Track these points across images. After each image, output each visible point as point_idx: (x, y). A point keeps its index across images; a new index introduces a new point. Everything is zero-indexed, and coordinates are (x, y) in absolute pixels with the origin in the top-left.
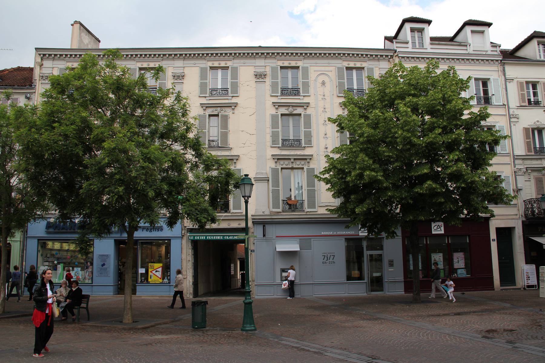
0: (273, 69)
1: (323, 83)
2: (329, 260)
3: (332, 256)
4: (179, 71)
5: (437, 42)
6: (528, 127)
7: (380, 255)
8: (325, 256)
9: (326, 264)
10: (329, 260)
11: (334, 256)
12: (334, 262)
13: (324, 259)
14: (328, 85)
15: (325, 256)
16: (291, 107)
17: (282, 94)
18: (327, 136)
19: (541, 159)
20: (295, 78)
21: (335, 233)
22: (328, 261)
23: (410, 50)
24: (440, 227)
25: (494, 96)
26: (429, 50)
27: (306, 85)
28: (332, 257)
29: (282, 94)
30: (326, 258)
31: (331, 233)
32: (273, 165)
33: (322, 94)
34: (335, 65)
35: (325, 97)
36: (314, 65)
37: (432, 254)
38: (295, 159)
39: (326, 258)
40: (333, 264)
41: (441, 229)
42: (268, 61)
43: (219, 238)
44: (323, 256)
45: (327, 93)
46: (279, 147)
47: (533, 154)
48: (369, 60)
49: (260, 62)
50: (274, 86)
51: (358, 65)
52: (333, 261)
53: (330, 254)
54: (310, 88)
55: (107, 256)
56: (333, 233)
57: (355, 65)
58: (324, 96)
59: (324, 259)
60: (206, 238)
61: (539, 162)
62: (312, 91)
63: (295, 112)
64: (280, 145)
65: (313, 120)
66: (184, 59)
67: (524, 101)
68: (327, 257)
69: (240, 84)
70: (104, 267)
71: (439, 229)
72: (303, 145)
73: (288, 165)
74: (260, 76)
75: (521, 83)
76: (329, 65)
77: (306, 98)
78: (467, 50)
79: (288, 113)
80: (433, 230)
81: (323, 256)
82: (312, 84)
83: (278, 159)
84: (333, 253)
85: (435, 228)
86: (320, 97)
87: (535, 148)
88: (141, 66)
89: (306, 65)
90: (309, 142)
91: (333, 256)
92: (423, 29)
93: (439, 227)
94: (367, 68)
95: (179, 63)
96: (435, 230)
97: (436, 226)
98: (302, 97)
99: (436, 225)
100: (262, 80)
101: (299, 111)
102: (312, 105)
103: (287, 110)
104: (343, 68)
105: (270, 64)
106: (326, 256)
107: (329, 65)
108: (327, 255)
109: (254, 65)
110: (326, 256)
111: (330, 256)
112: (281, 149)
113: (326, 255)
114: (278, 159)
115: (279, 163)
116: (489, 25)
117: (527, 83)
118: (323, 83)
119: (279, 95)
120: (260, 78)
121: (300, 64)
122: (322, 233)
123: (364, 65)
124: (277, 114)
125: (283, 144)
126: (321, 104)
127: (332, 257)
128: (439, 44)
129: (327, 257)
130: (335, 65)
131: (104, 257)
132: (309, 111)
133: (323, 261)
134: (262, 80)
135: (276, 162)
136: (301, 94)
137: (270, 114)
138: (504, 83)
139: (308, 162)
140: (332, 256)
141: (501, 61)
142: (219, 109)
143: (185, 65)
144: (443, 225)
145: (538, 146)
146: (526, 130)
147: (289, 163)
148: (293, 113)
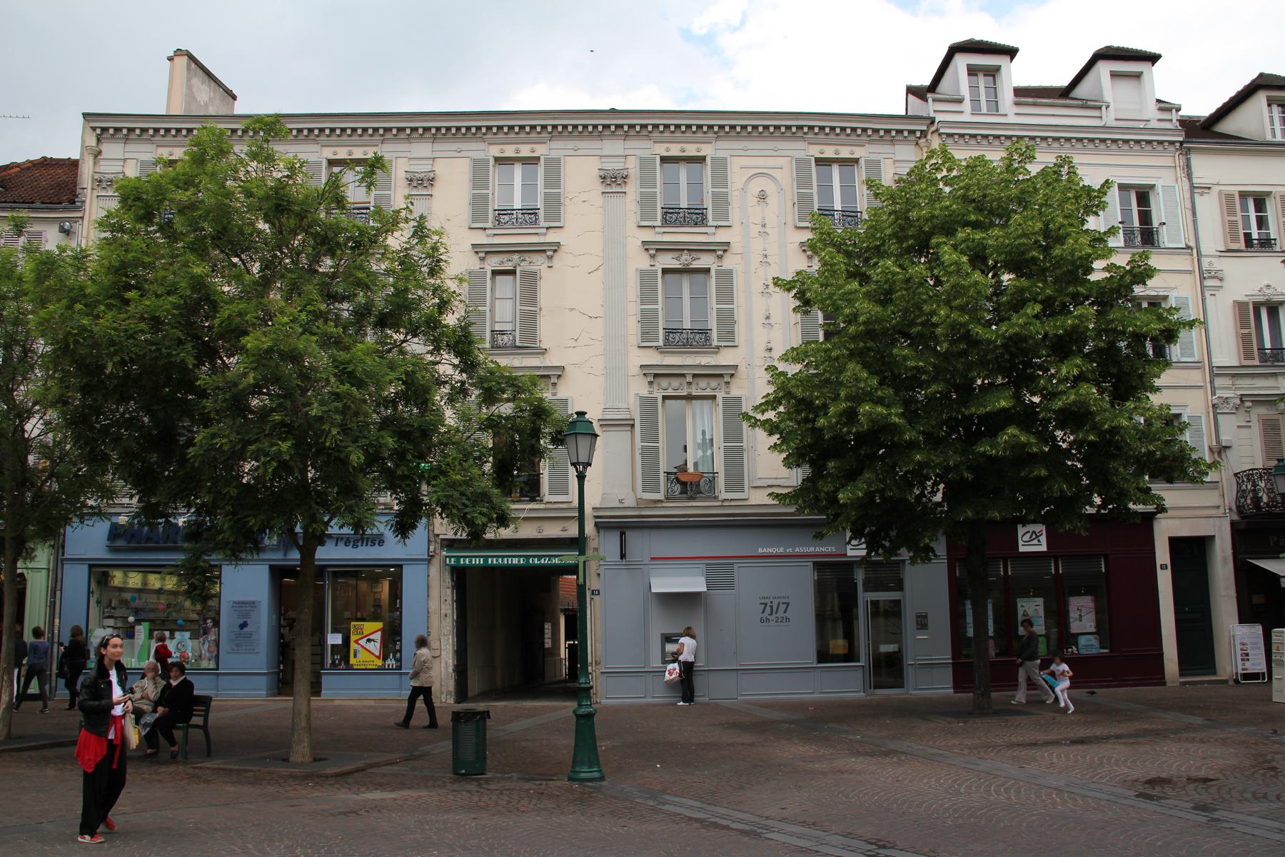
0: (645, 164)
1: (762, 197)
2: (776, 613)
3: (783, 603)
4: (421, 168)
5: (1030, 100)
6: (1246, 299)
7: (897, 603)
8: (766, 604)
9: (768, 624)
10: (776, 613)
11: (788, 604)
12: (788, 619)
13: (763, 612)
14: (773, 200)
15: (766, 604)
16: (686, 252)
17: (666, 222)
18: (771, 321)
19: (1275, 375)
20: (695, 185)
22: (774, 615)
23: (966, 117)
24: (1037, 536)
26: (1012, 119)
27: (722, 201)
28: (782, 607)
29: (666, 222)
30: (768, 609)
32: (644, 390)
33: (759, 221)
34: (790, 153)
35: (766, 230)
36: (741, 153)
37: (1018, 600)
38: (695, 376)
39: (768, 609)
40: (785, 623)
41: (1039, 541)
42: (631, 144)
43: (515, 561)
44: (761, 604)
45: (772, 220)
46: (657, 348)
47: (1257, 363)
48: (870, 142)
49: (613, 146)
50: (646, 202)
51: (845, 153)
52: (784, 615)
53: (779, 600)
54: (730, 207)
55: (253, 604)
57: (837, 153)
59: (763, 612)
60: (486, 561)
61: (1270, 382)
62: (735, 214)
63: (696, 265)
64: (661, 343)
65: (739, 283)
66: (434, 139)
67: (1235, 239)
68: (772, 607)
69: (565, 198)
70: (245, 629)
71: (1035, 542)
72: (715, 343)
73: (680, 391)
74: (612, 180)
75: (1229, 197)
76: (775, 154)
77: (721, 231)
78: (1101, 117)
80: (1020, 543)
81: (761, 604)
82: (735, 199)
83: (656, 376)
84: (784, 598)
85: (1027, 538)
86: (755, 230)
87: (1261, 349)
88: (332, 157)
89: (721, 154)
91: (785, 605)
92: (998, 69)
93: (1034, 536)
94: (866, 161)
95: (422, 149)
96: (1027, 543)
97: (1029, 535)
99: (1029, 532)
100: (618, 189)
101: (705, 261)
102: (735, 247)
103: (678, 259)
104: (808, 162)
105: (637, 152)
106: (769, 604)
107: (775, 154)
108: (771, 602)
109: (599, 152)
110: (769, 604)
111: (779, 603)
112: (661, 353)
113: (768, 601)
114: (655, 375)
115: (659, 384)
116: (1153, 58)
117: (1243, 195)
118: (762, 197)
119: (659, 223)
120: (614, 185)
121: (707, 150)
123: (858, 152)
124: (653, 268)
126: (757, 245)
127: (782, 607)
128: (1035, 105)
129: (772, 607)
130: (790, 153)
131: (245, 607)
132: (729, 262)
133: (763, 615)
134: (618, 189)
135: (651, 383)
136: (711, 223)
137: (637, 269)
138: (1187, 195)
139: (726, 383)
140: (783, 603)
141: (1181, 143)
142: (516, 257)
143: (435, 155)
144: (1044, 532)
145: (1268, 344)
146: (1240, 306)
147: (681, 384)
148: (691, 266)
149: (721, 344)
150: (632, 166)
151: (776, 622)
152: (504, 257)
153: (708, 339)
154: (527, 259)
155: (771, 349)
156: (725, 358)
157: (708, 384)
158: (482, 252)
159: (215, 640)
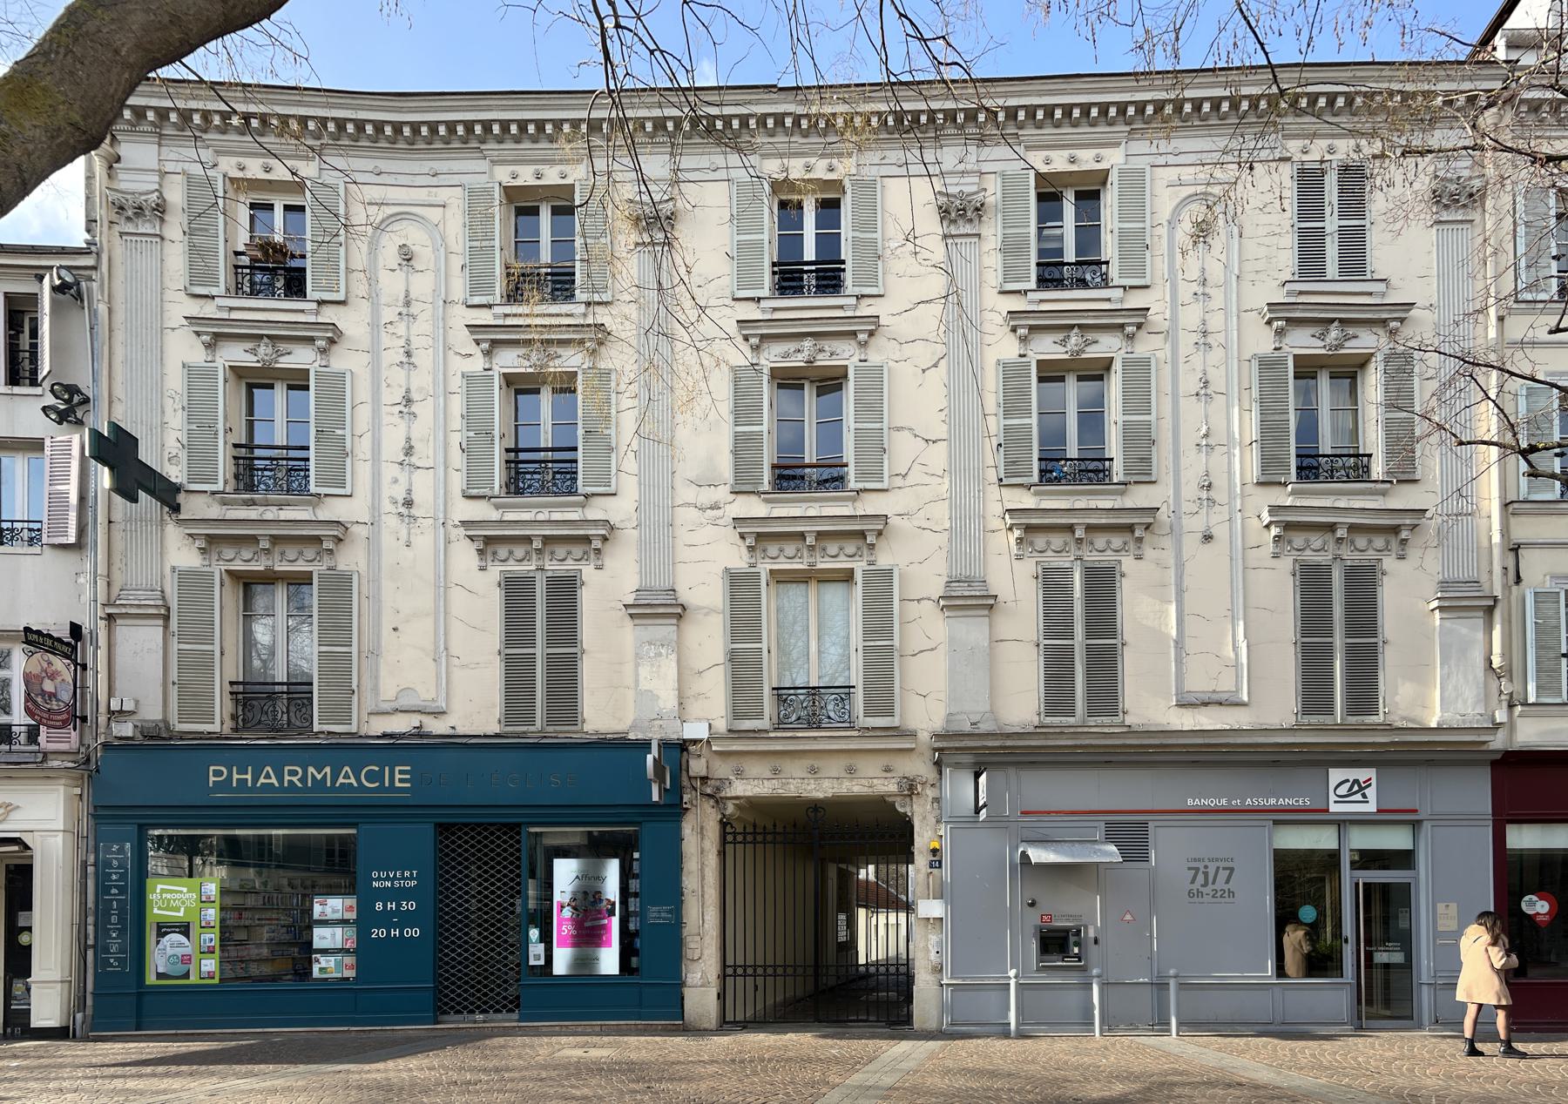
1: (407, 257)
2: (1213, 883)
3: (1224, 869)
8: (1197, 869)
9: (1200, 899)
10: (1213, 883)
11: (1232, 870)
12: (1231, 893)
13: (1193, 882)
15: (1197, 869)
16: (1076, 330)
17: (1044, 282)
21: (1236, 803)
22: (1210, 887)
24: (1361, 789)
25: (1554, 254)
28: (1223, 875)
30: (1201, 878)
31: (1224, 802)
32: (738, 559)
35: (1207, 290)
39: (1201, 878)
40: (1227, 900)
41: (1364, 796)
44: (1189, 869)
50: (1011, 248)
52: (1226, 887)
53: (1218, 864)
56: (1229, 801)
58: (1204, 282)
59: (1193, 882)
62: (1157, 266)
65: (1161, 381)
68: (1206, 874)
69: (884, 249)
71: (1358, 797)
72: (313, 489)
73: (253, 563)
76: (434, 181)
79: (1323, 352)
80: (1332, 798)
81: (1189, 869)
84: (1226, 860)
85: (1343, 790)
86: (1186, 291)
90: (1142, 472)
91: (1193, 872)
93: (1356, 788)
96: (1342, 799)
97: (1348, 785)
98: (1119, 293)
99: (1348, 781)
100: (968, 229)
104: (488, 192)
106: (1202, 869)
107: (434, 181)
108: (1206, 867)
110: (1202, 869)
111: (1218, 868)
112: (767, 501)
113: (1201, 865)
114: (761, 537)
115: (283, 554)
118: (407, 257)
119: (1033, 285)
120: (960, 222)
121: (1113, 158)
122: (1190, 802)
124: (1023, 360)
125: (1041, 477)
126: (1191, 317)
127: (1223, 875)
129: (1206, 874)
130: (465, 179)
132: (340, 361)
133: (1192, 886)
135: (751, 549)
139: (595, 549)
140: (1224, 869)
142: (808, 344)
144: (1374, 782)
147: (858, 549)
148: (1084, 356)
149: (1128, 479)
150: (993, 192)
151: (1213, 897)
152: (790, 346)
153: (1367, 469)
154: (827, 348)
155: (1210, 486)
156: (1139, 497)
157: (1370, 541)
158: (1022, 326)
159: (255, 888)
